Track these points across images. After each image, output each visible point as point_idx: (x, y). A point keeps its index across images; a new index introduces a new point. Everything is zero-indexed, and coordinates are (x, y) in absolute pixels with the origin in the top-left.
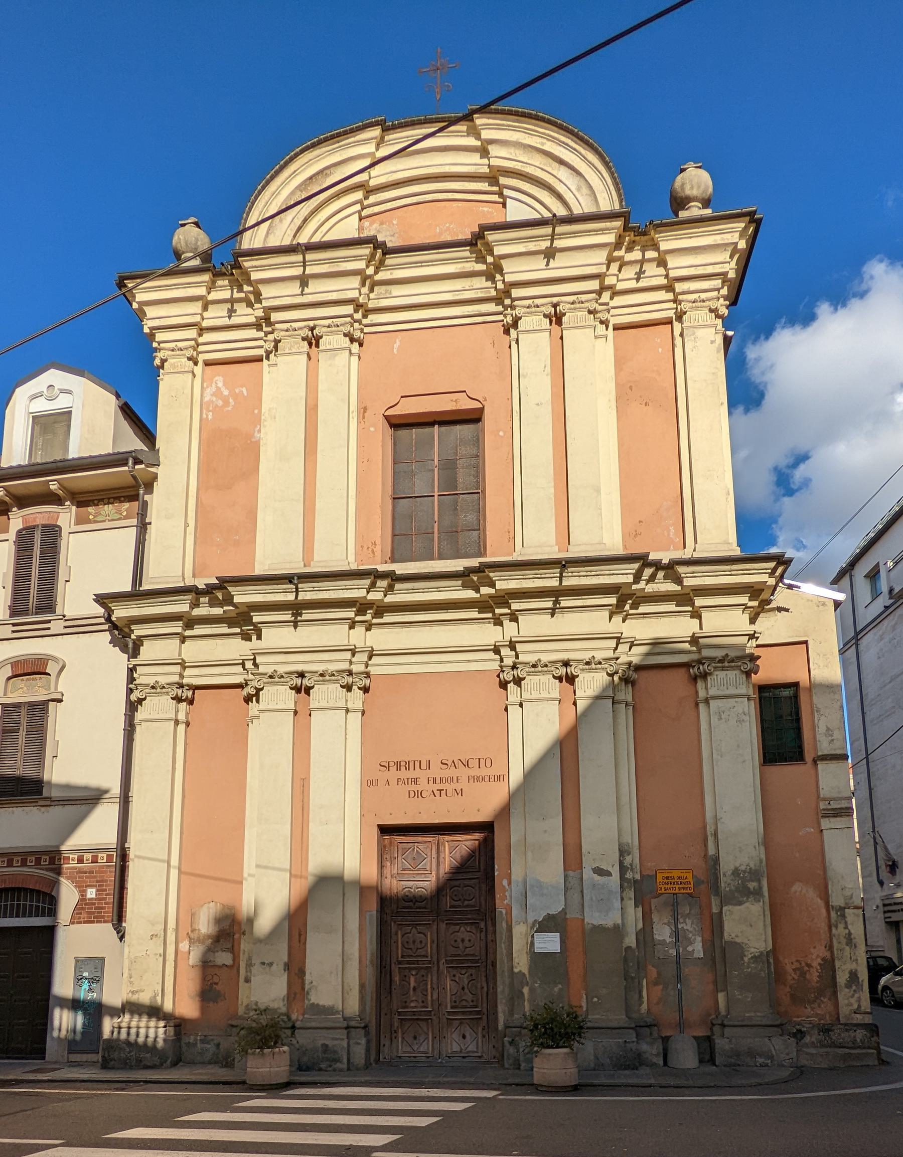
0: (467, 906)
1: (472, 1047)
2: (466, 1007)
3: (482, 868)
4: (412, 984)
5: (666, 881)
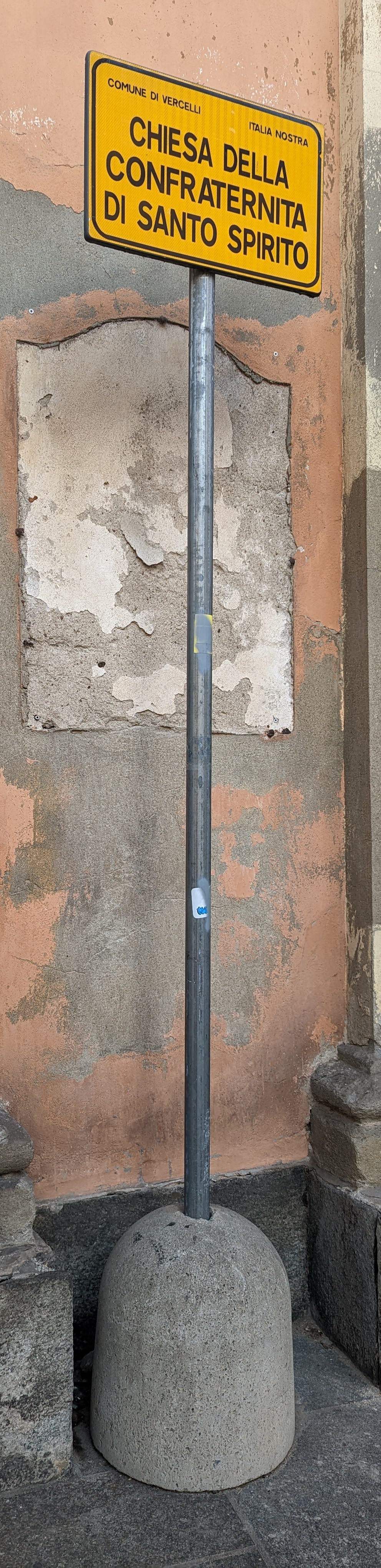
5: (160, 159)
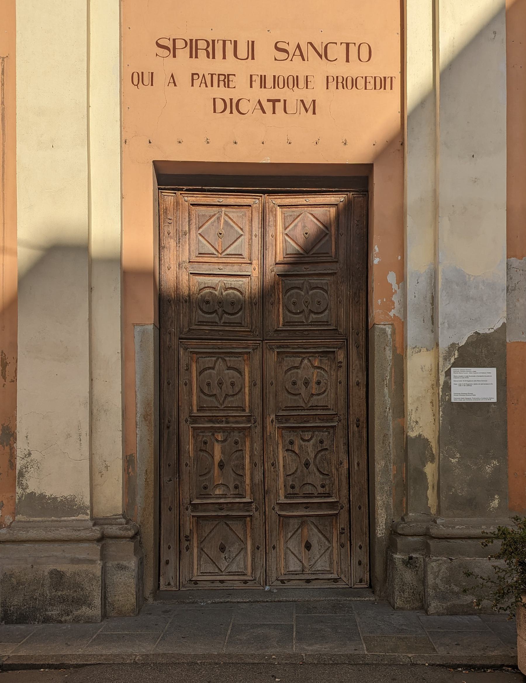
0: (314, 323)
1: (322, 564)
2: (310, 496)
3: (341, 258)
4: (218, 456)
